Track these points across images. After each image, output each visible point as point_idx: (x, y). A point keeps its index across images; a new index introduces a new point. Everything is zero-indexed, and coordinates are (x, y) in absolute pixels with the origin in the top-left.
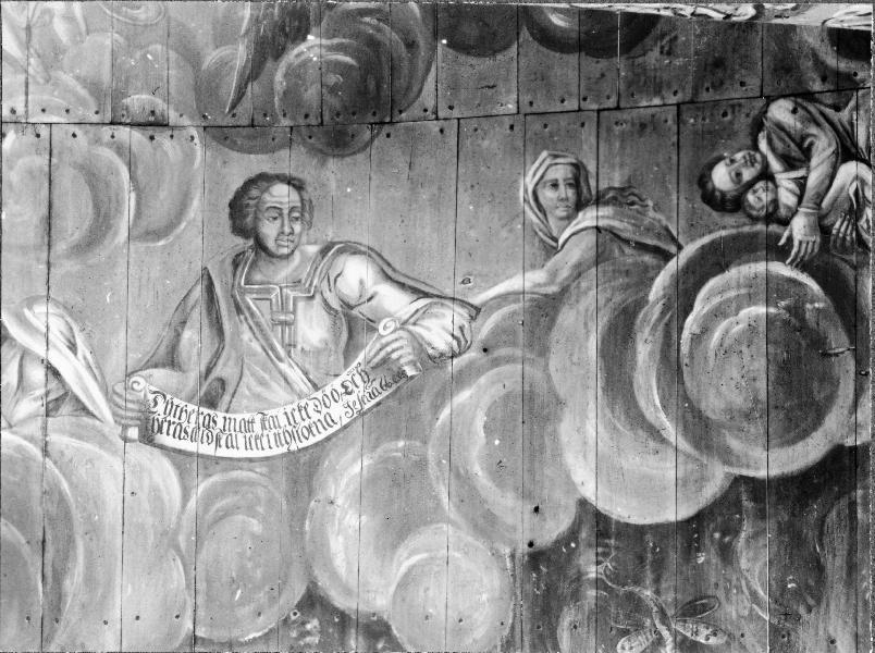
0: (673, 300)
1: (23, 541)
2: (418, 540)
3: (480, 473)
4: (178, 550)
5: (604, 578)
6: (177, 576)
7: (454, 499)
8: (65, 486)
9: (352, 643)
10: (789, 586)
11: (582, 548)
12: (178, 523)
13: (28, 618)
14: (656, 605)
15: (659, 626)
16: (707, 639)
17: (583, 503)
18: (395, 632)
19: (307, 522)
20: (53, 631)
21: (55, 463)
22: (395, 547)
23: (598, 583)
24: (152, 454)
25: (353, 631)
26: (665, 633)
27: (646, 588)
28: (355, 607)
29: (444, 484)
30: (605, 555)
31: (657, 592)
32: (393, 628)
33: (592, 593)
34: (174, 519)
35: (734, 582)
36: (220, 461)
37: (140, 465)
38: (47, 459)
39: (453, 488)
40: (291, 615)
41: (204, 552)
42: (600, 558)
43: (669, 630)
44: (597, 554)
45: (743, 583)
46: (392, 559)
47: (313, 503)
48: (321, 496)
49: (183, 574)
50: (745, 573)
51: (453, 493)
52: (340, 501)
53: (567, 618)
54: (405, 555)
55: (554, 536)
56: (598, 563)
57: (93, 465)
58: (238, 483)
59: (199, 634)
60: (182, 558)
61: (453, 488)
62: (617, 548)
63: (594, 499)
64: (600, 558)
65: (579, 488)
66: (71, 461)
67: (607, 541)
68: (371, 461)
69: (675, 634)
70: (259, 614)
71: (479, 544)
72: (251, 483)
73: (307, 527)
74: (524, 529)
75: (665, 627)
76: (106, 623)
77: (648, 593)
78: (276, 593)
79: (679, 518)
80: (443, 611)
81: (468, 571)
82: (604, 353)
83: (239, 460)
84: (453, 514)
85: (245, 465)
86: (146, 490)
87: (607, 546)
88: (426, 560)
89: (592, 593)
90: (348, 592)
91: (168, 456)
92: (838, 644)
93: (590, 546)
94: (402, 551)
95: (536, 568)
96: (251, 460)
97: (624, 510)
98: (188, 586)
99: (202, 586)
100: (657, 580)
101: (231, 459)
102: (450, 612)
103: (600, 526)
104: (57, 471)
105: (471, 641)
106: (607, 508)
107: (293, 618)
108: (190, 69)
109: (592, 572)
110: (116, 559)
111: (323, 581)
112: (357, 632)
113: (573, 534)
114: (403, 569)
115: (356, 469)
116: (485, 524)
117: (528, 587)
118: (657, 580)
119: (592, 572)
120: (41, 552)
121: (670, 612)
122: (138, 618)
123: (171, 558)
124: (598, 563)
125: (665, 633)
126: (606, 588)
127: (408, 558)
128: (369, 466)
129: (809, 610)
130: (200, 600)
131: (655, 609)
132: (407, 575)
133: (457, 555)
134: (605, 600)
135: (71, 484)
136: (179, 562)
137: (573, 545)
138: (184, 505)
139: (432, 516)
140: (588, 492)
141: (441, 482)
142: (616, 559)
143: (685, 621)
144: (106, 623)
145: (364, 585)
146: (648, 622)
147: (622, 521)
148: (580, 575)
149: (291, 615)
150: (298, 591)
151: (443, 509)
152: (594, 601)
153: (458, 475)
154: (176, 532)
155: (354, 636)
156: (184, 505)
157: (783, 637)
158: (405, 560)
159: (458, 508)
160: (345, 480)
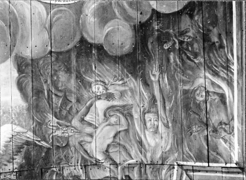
0: (217, 89)
1: (5, 25)
2: (109, 24)
3: (126, 5)
4: (46, 28)
5: (160, 29)
6: (46, 36)
7: (119, 12)
8: (15, 11)
9: (94, 52)
10: (208, 22)
11: (153, 22)
12: (46, 22)
13: (7, 46)
14: (173, 34)
15: (174, 39)
16: (187, 40)
17: (153, 10)
18: (105, 48)
19: (80, 20)
20: (13, 49)
21: (12, 5)
22: (104, 26)
23: (158, 30)
24: (38, 3)
25: (94, 49)
26: (176, 41)
27: (171, 29)
28: (94, 42)
29: (117, 9)
30: (160, 23)
31: (174, 30)
32: (104, 47)
33: (156, 33)
34: (45, 21)
35: (194, 24)
36: (57, 5)
37: (35, 7)
38: (10, 4)
39: (119, 10)
40: (77, 45)
41: (53, 28)
42: (158, 24)
43: (177, 39)
44: (157, 23)
45: (196, 23)
46: (103, 29)
47: (82, 16)
48: (84, 14)
49: (48, 35)
50: (197, 21)
51: (119, 11)
52: (89, 15)
53: (150, 40)
54: (107, 28)
55: (146, 19)
56: (158, 25)
57: (23, 6)
58: (61, 10)
59: (53, 50)
60: (47, 30)
61: (119, 10)
62: (163, 20)
63: (156, 8)
64: (158, 24)
65: (152, 6)
66: (16, 4)
67: (160, 19)
68: (97, 4)
69: (179, 40)
70: (68, 45)
71: (126, 24)
72: (65, 11)
73: (80, 22)
74: (138, 18)
75: (176, 39)
76: (27, 47)
77: (171, 31)
78: (73, 39)
79: (179, 10)
80: (117, 42)
81: (124, 31)
82: (189, 60)
83: (62, 5)
84: (119, 17)
85: (63, 6)
86: (37, 13)
87: (160, 20)
88: (113, 29)
89: (156, 33)
90: (92, 39)
91: (42, 4)
92: (222, 35)
93: (156, 21)
94: (106, 27)
95: (142, 29)
96: (65, 5)
97: (164, 9)
98: (49, 38)
99: (53, 38)
100: (173, 27)
101: (59, 4)
102: (119, 42)
103: (156, 14)
104: (13, 7)
105: (125, 49)
106: (159, 10)
107: (77, 46)
108: (119, 53)
109: (156, 27)
110: (29, 33)
111: (85, 36)
112: (95, 49)
113: (151, 18)
114: (106, 32)
115: (93, 6)
116: (128, 18)
117: (139, 34)
118: (173, 27)
119: (156, 27)
120: (9, 29)
121: (177, 35)
122: (36, 46)
123: (44, 31)
124: (158, 25)
125: (176, 41)
126: (161, 31)
127: (107, 29)
128: (96, 6)
129: (214, 28)
130: (52, 41)
131: (173, 35)
132: (107, 33)
133: (120, 27)
134: (160, 34)
135: (16, 10)
136: (47, 32)
137: (151, 21)
138: (47, 17)
139: (114, 17)
140: (155, 7)
141: (116, 8)
142: (163, 23)
143: (181, 36)
144: (27, 47)
145: (96, 37)
146: (172, 39)
147: (164, 13)
148: (153, 28)
149: (77, 45)
150: (78, 38)
151: (116, 15)
152: (157, 35)
153: (120, 6)
154: (45, 24)
155: (94, 50)
156: (47, 17)
157: (207, 36)
158: (108, 29)
159: (120, 14)
160: (90, 9)
